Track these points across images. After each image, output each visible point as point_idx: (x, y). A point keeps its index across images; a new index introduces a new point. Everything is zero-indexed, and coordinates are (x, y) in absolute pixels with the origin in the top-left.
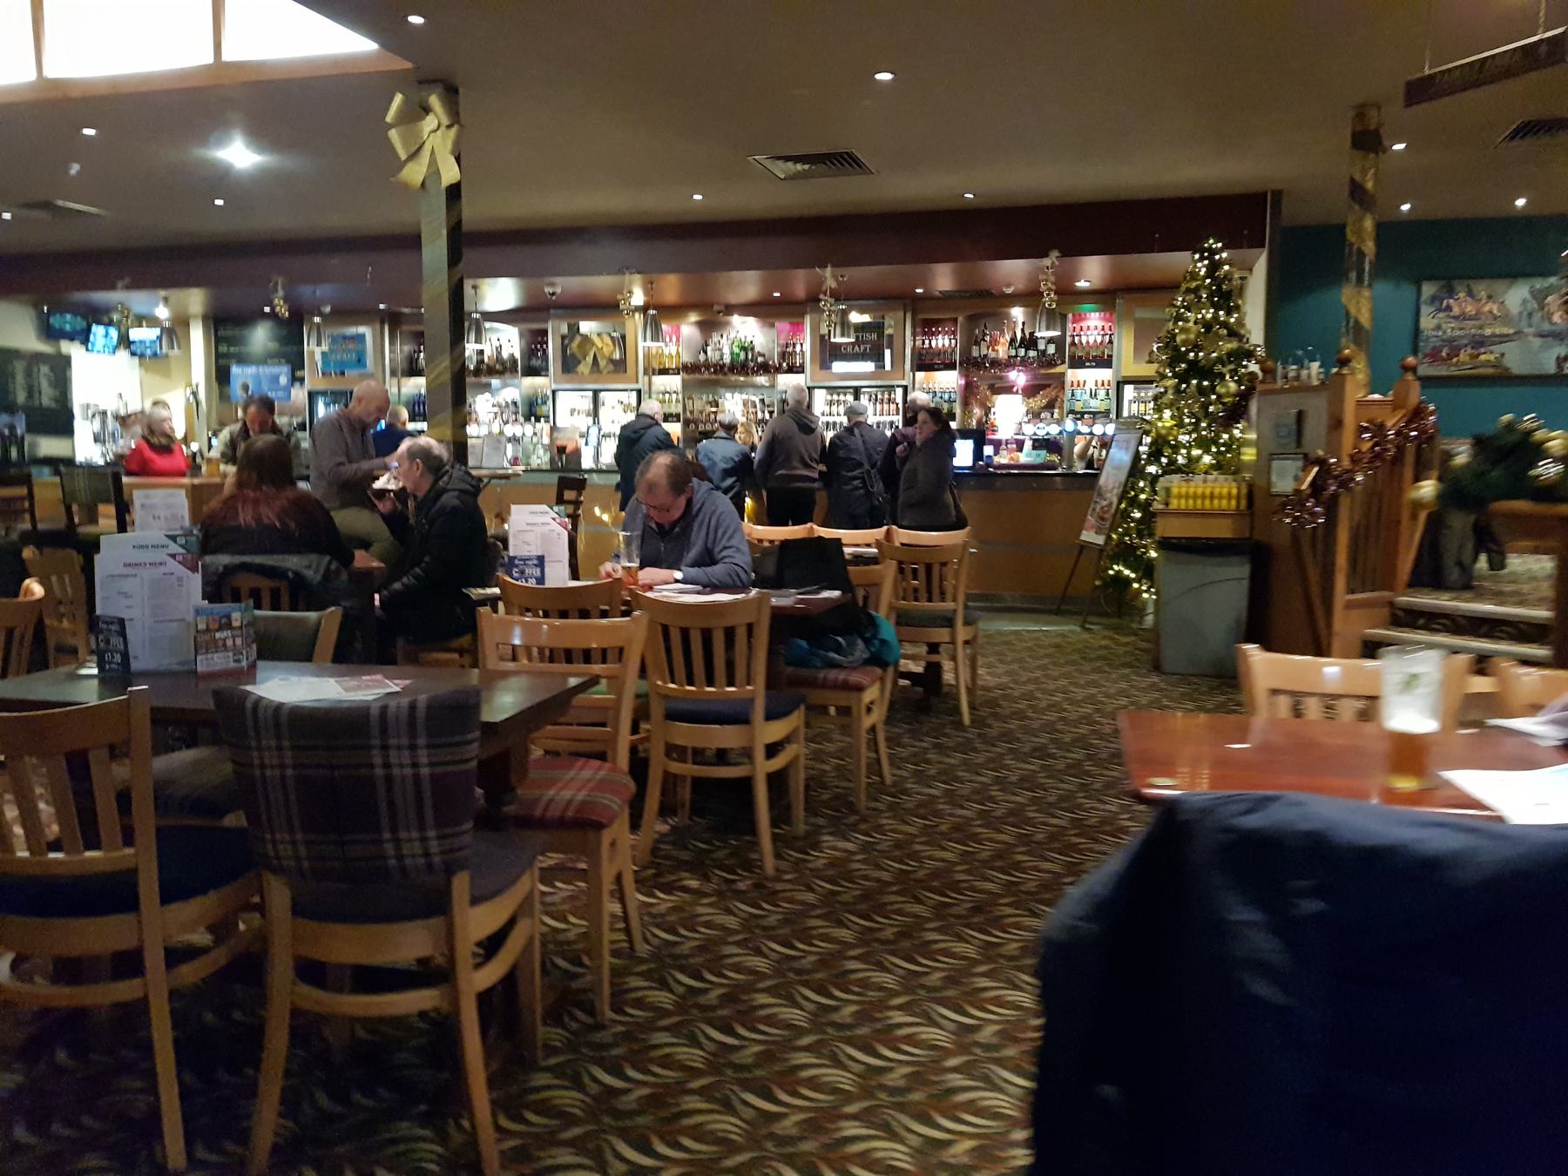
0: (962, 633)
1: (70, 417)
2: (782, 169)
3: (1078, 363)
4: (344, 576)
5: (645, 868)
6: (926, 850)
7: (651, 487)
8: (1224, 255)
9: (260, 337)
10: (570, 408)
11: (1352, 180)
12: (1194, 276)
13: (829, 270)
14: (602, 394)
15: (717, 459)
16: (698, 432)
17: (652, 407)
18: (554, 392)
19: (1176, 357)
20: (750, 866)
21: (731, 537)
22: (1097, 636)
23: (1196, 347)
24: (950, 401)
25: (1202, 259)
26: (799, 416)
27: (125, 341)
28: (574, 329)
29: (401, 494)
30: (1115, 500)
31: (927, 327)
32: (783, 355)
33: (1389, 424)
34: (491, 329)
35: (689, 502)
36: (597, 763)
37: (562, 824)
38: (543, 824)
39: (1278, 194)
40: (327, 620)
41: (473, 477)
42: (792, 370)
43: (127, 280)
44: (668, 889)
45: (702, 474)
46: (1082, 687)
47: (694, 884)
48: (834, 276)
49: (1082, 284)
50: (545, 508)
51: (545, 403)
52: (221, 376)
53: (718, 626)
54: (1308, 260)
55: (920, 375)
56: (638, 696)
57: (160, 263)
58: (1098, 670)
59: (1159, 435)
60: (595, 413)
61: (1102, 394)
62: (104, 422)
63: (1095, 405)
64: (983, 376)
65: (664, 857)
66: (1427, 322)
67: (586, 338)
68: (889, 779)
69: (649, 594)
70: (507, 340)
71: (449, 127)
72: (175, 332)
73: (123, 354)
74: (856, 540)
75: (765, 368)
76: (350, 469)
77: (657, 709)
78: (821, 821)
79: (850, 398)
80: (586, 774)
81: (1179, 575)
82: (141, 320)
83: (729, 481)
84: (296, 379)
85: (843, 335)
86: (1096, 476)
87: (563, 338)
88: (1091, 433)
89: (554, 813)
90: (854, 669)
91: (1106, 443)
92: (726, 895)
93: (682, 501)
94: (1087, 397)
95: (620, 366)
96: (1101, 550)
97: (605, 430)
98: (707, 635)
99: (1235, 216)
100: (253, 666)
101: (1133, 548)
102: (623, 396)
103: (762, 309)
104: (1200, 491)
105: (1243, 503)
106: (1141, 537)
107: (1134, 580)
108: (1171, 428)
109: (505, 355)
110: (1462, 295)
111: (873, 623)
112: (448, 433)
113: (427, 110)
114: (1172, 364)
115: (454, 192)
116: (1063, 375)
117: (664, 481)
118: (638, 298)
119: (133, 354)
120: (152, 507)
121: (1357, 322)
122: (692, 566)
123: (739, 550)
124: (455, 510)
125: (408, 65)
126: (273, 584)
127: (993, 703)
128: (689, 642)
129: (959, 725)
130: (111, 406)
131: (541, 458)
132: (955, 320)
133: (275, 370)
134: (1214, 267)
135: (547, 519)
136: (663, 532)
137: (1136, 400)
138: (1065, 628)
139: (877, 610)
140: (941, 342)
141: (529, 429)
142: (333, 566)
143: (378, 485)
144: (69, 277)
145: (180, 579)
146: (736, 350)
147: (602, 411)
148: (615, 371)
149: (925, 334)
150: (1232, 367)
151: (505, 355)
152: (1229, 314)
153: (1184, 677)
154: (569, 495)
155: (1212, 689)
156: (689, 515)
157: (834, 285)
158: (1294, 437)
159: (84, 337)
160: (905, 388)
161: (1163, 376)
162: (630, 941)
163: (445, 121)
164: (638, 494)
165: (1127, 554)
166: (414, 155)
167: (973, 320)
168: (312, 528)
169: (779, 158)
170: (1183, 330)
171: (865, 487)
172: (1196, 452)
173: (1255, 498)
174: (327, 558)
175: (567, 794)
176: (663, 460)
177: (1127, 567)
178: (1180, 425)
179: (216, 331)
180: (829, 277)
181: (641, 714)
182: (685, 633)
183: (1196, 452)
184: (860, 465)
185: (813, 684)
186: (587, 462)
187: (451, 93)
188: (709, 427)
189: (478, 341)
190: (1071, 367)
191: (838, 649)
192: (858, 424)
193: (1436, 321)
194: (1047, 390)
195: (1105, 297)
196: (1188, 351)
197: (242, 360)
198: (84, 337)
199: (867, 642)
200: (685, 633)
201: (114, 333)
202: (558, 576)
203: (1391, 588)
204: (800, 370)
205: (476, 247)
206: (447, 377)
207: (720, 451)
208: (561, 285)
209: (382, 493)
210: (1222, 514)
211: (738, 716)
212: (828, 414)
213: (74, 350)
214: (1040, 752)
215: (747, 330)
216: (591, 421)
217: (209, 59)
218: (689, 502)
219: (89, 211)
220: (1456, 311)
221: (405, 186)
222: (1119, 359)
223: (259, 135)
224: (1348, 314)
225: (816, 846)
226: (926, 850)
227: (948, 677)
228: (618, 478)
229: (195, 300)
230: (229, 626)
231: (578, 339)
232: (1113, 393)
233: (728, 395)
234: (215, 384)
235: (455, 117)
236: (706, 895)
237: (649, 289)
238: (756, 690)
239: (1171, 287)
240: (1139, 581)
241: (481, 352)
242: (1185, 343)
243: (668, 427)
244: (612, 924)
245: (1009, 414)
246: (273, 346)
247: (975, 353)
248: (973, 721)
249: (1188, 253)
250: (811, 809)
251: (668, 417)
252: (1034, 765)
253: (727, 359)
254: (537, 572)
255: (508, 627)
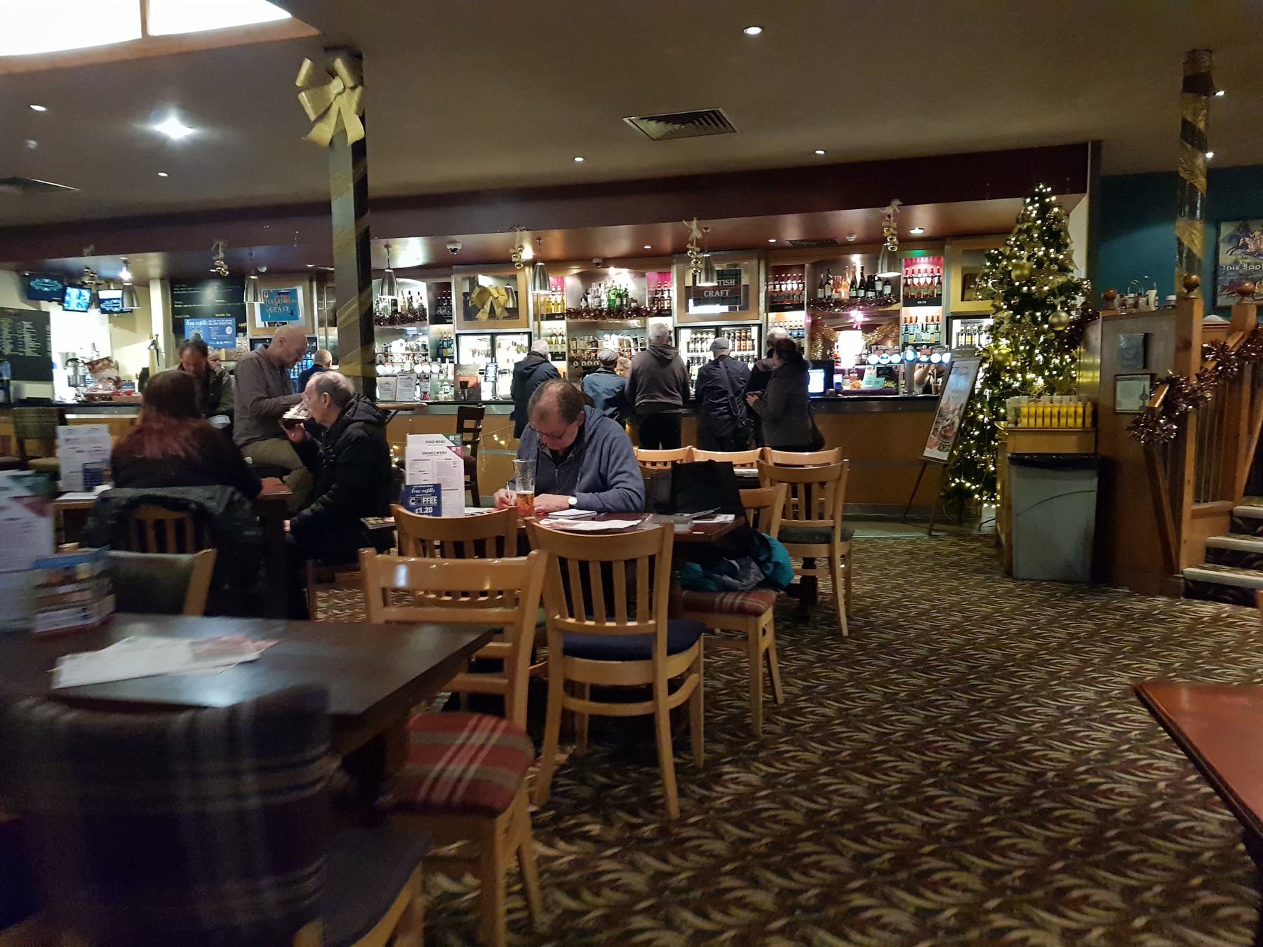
0: (840, 548)
1: (51, 365)
2: (653, 127)
3: (911, 302)
4: (248, 506)
5: (544, 809)
6: (834, 784)
7: (543, 415)
8: (1054, 198)
9: (211, 295)
10: (471, 351)
11: (1185, 122)
12: (1025, 218)
13: (695, 221)
14: (498, 338)
15: (600, 390)
16: (582, 369)
17: (541, 346)
18: (457, 336)
19: (1011, 292)
20: (654, 805)
21: (622, 464)
22: (945, 544)
23: (1030, 282)
24: (798, 337)
25: (1033, 202)
26: (662, 352)
27: (96, 301)
28: (474, 283)
29: (310, 424)
30: (957, 421)
31: (778, 273)
32: (653, 300)
33: (1231, 344)
34: (403, 284)
35: (582, 429)
36: (489, 721)
37: (448, 808)
38: (427, 808)
39: (1097, 145)
40: (198, 562)
41: (377, 409)
42: (661, 313)
43: (92, 248)
44: (569, 836)
45: (591, 402)
46: (944, 593)
47: (595, 829)
48: (699, 228)
49: (916, 232)
50: (441, 437)
51: (450, 346)
52: (177, 328)
53: (619, 557)
54: (1130, 200)
55: (772, 315)
56: (538, 626)
57: (122, 231)
58: (954, 577)
59: (995, 362)
60: (493, 354)
61: (932, 328)
62: (76, 367)
63: (927, 337)
64: (826, 313)
65: (564, 795)
66: (1225, 258)
67: (484, 291)
68: (781, 698)
69: (544, 523)
70: (418, 293)
71: (353, 88)
72: (137, 289)
73: (94, 312)
74: (743, 461)
75: (638, 312)
76: (269, 403)
77: (555, 644)
78: (720, 748)
79: (712, 336)
80: (478, 738)
81: (1028, 490)
82: (110, 282)
83: (611, 410)
84: (240, 330)
85: (707, 280)
86: (937, 399)
87: (465, 294)
88: (929, 362)
89: (440, 795)
90: (749, 592)
91: (943, 372)
92: (630, 843)
93: (574, 429)
94: (919, 331)
95: (513, 313)
96: (945, 465)
97: (501, 367)
98: (607, 568)
99: (1062, 165)
100: (106, 623)
101: (973, 462)
102: (517, 338)
103: (636, 261)
104: (1048, 410)
105: (1088, 421)
106: (981, 452)
107: (975, 491)
108: (1008, 354)
109: (416, 305)
110: (1257, 234)
111: (766, 545)
112: (357, 369)
113: (333, 74)
114: (1006, 299)
115: (359, 149)
116: (899, 311)
117: (556, 409)
118: (528, 253)
119: (104, 311)
120: (76, 441)
121: (1190, 251)
122: (586, 491)
123: (631, 475)
124: (359, 439)
125: (313, 31)
126: (177, 515)
127: (865, 611)
128: (588, 574)
129: (837, 635)
130: (86, 354)
131: (447, 393)
132: (803, 266)
133: (222, 322)
134: (1044, 209)
135: (443, 448)
136: (558, 458)
137: (966, 333)
138: (914, 535)
139: (768, 533)
140: (790, 286)
141: (435, 368)
142: (237, 496)
143: (288, 415)
144: (45, 247)
145: (28, 524)
146: (613, 297)
147: (498, 352)
148: (509, 317)
149: (776, 279)
150: (1063, 298)
151: (416, 305)
152: (1058, 251)
153: (1036, 583)
154: (469, 424)
155: (1067, 594)
156: (580, 442)
157: (699, 236)
158: (1141, 359)
159: (60, 298)
160: (760, 326)
161: (999, 309)
162: (527, 907)
163: (350, 83)
164: (532, 423)
165: (967, 468)
166: (323, 116)
167: (817, 266)
168: (220, 460)
169: (651, 119)
170: (1016, 267)
171: (730, 412)
172: (1030, 376)
173: (1100, 414)
174: (230, 489)
175: (456, 769)
176: (554, 388)
177: (968, 480)
178: (1015, 352)
179: (172, 291)
180: (695, 229)
181: (541, 640)
182: (584, 566)
183: (1030, 376)
184: (725, 393)
185: (710, 609)
186: (486, 395)
187: (356, 61)
188: (590, 363)
189: (391, 293)
190: (905, 305)
191: (733, 573)
192: (722, 357)
193: (1233, 258)
194: (884, 323)
195: (935, 244)
196: (1022, 285)
197: (195, 315)
198: (60, 298)
199: (761, 565)
200: (584, 566)
201: (86, 294)
202: (456, 505)
203: (1232, 500)
204: (668, 313)
205: (383, 211)
206: (356, 318)
207: (603, 383)
208: (463, 242)
209: (292, 423)
210: (1068, 432)
211: (639, 651)
212: (693, 352)
213: (53, 309)
214: (921, 664)
215: (621, 279)
216: (489, 362)
217: (138, 35)
218: (582, 429)
219: (68, 192)
220: (1252, 248)
221: (314, 145)
222: (948, 295)
223: (192, 112)
224: (1180, 244)
225: (718, 778)
226: (834, 784)
227: (823, 586)
228: (512, 408)
229: (153, 263)
230: (69, 579)
231: (477, 290)
232: (942, 327)
233: (607, 336)
234: (172, 335)
235: (359, 80)
236: (609, 845)
237: (537, 246)
238: (659, 624)
239: (1002, 232)
240: (980, 493)
241: (395, 303)
242: (1018, 278)
243: (555, 364)
244: (508, 886)
245: (849, 347)
246: (219, 302)
247: (820, 295)
248: (850, 631)
249: (1020, 200)
250: (711, 737)
251: (555, 356)
252: (919, 680)
253: (605, 305)
254: (433, 500)
255: (392, 568)
